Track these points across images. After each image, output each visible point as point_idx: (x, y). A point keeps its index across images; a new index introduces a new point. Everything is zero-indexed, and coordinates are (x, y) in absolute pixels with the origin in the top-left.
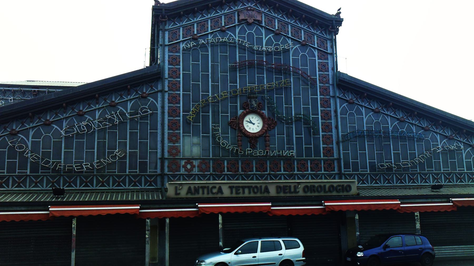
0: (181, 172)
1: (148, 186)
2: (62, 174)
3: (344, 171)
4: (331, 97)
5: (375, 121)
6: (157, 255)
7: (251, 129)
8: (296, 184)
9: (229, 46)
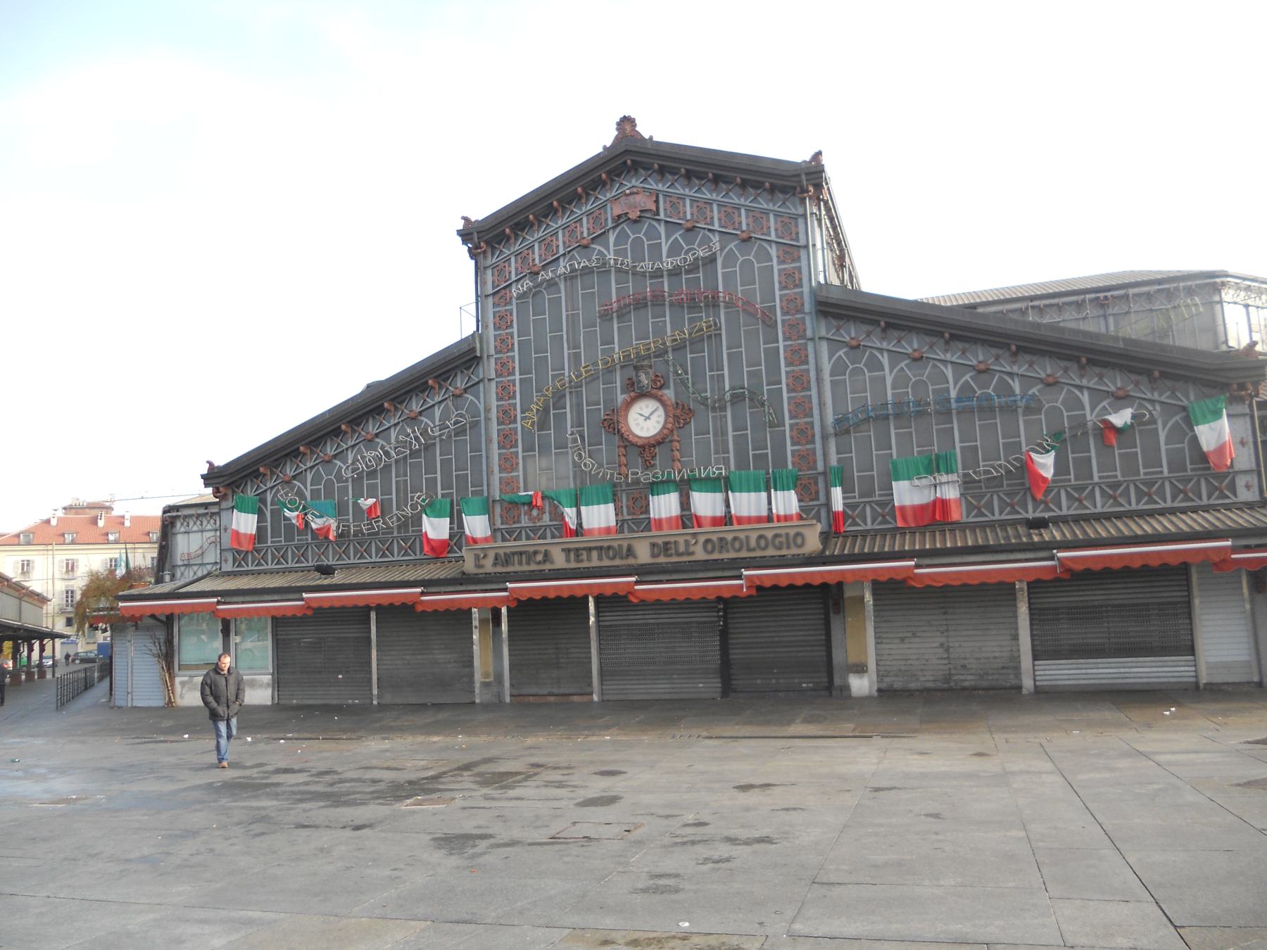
0: (523, 524)
1: (974, 517)
2: (351, 538)
4: (809, 339)
5: (914, 380)
6: (491, 670)
7: (645, 429)
8: (689, 538)
9: (598, 272)
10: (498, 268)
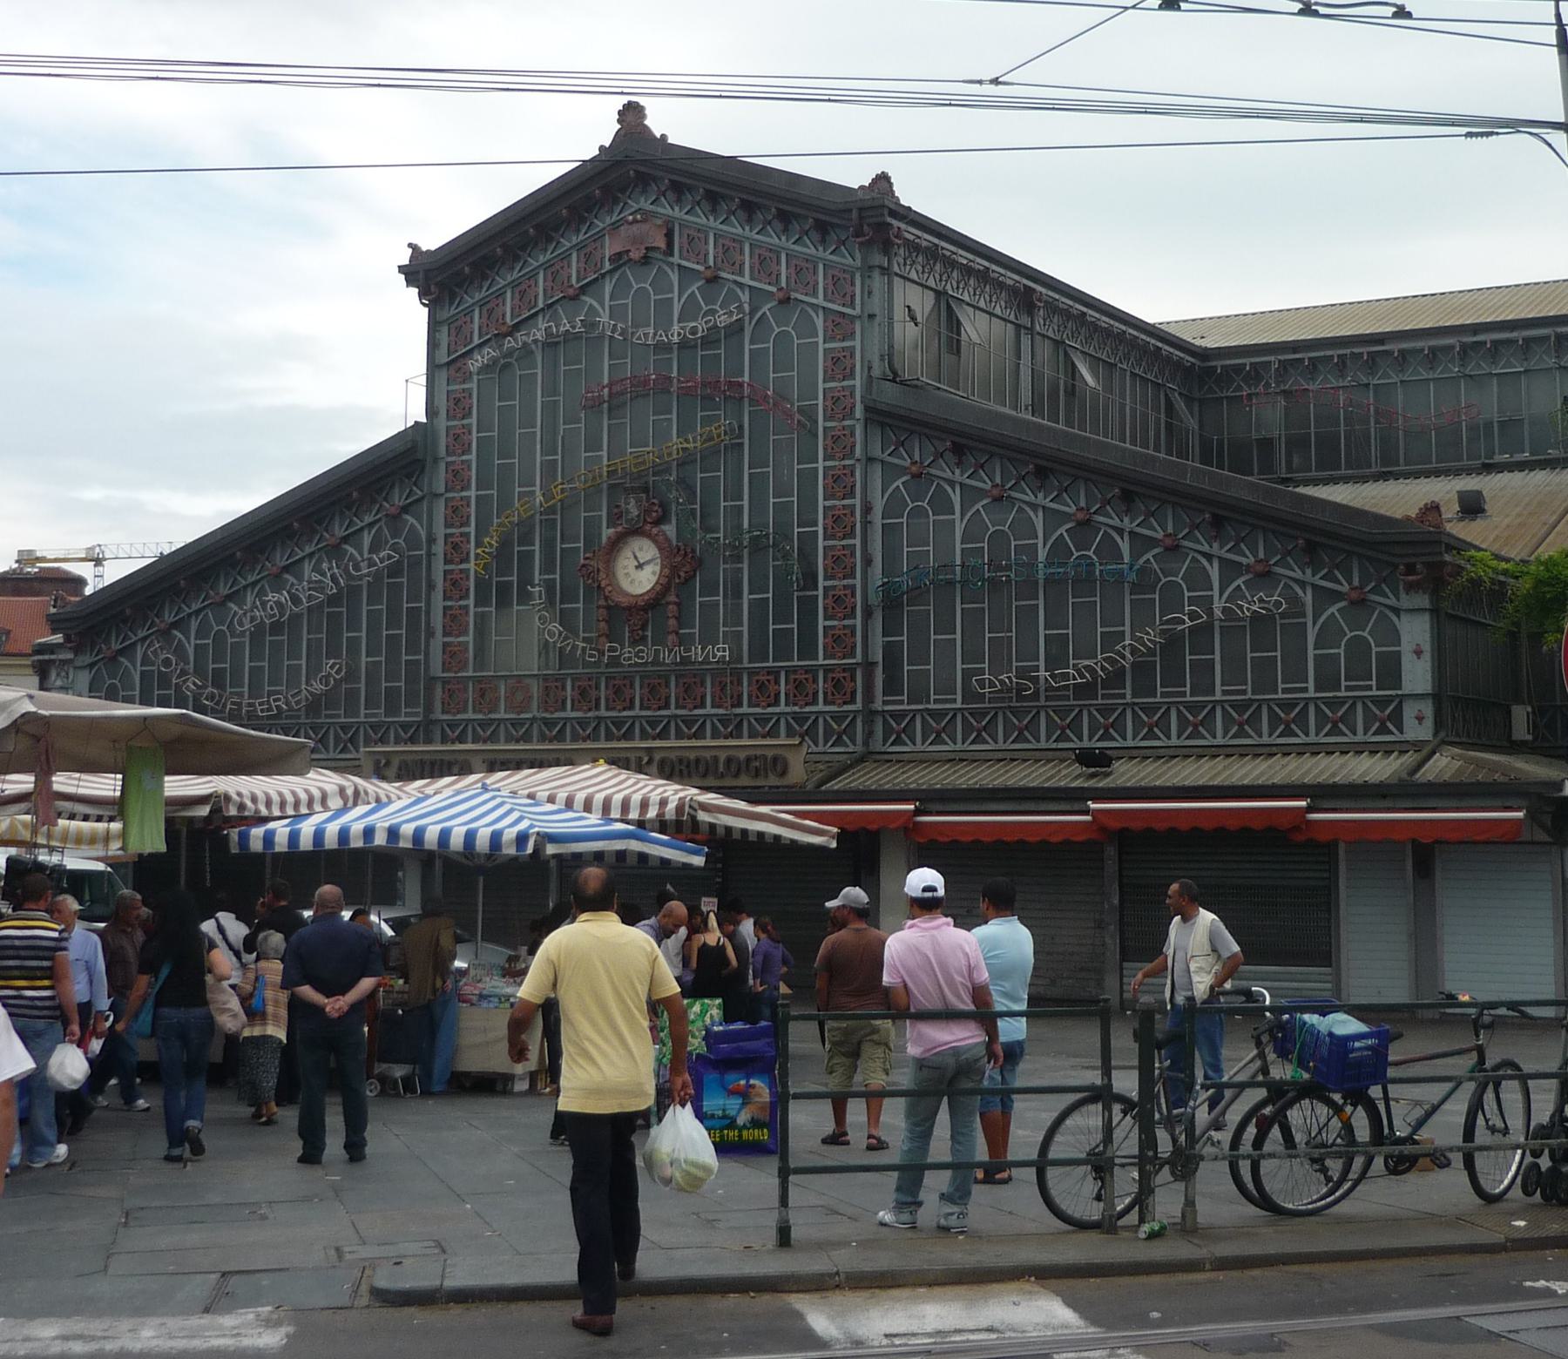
3: (1223, 691)
10: (456, 324)
